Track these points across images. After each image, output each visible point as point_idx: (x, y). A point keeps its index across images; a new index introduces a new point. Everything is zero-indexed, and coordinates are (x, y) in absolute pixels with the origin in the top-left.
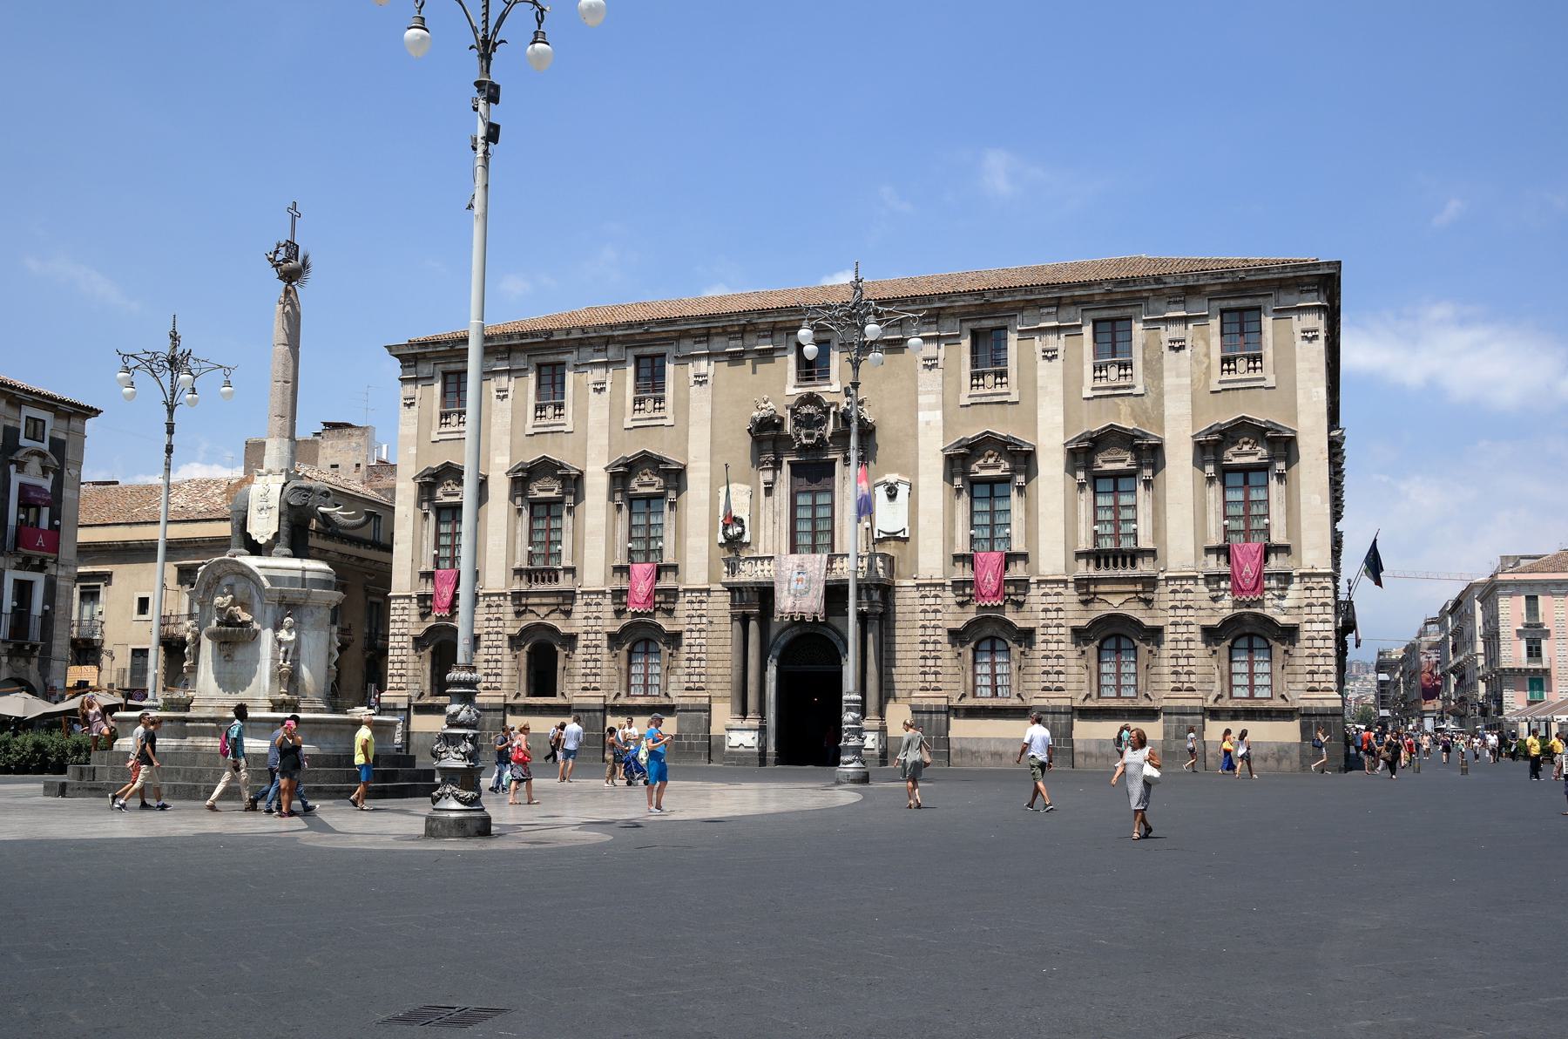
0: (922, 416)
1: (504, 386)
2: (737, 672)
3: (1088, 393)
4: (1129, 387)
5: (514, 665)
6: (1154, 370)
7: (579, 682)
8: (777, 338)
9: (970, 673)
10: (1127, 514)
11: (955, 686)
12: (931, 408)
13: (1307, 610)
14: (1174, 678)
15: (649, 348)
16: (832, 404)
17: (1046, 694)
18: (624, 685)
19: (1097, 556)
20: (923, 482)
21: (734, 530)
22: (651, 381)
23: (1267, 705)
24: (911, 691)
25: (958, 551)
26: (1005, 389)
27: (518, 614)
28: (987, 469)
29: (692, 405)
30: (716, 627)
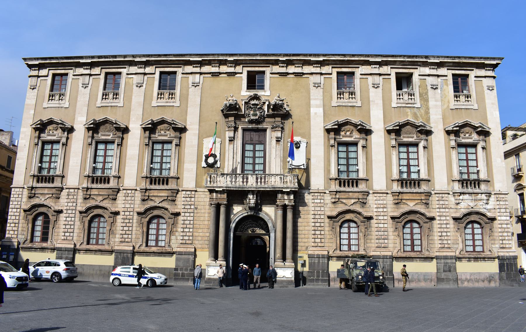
0: (313, 110)
1: (197, 80)
2: (212, 237)
3: (394, 105)
4: (414, 104)
5: (396, 234)
6: (424, 98)
7: (118, 238)
8: (237, 67)
9: (338, 238)
10: (473, 163)
11: (331, 245)
12: (317, 106)
13: (498, 210)
14: (440, 242)
15: (167, 69)
16: (266, 100)
17: (378, 249)
18: (145, 240)
19: (402, 182)
20: (313, 142)
21: (211, 160)
22: (112, 82)
23: (483, 255)
24: (307, 248)
25: (331, 177)
26: (413, 101)
27: (30, 197)
28: (345, 135)
29: (190, 97)
30: (199, 211)
